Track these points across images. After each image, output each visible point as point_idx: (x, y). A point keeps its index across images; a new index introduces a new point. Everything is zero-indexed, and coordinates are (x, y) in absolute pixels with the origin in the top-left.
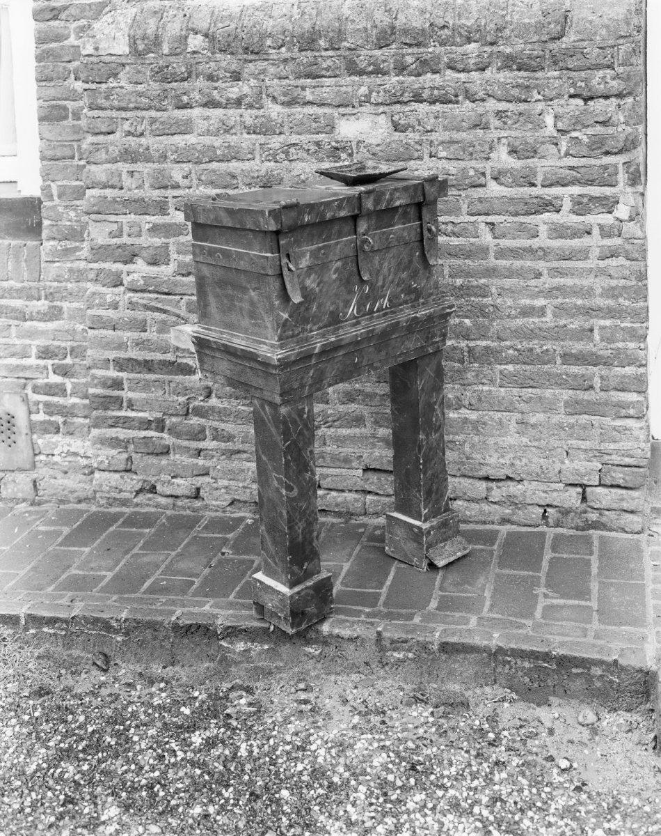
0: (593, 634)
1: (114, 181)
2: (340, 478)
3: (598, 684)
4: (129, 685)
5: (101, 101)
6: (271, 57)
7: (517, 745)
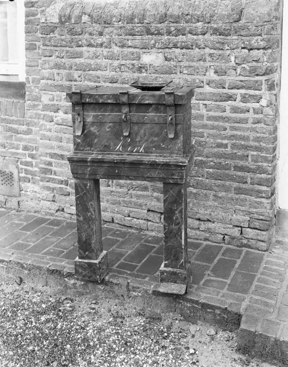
0: (222, 295)
1: (51, 77)
2: (137, 213)
3: (218, 318)
4: (26, 292)
5: (47, 43)
6: (115, 26)
7: (175, 340)
